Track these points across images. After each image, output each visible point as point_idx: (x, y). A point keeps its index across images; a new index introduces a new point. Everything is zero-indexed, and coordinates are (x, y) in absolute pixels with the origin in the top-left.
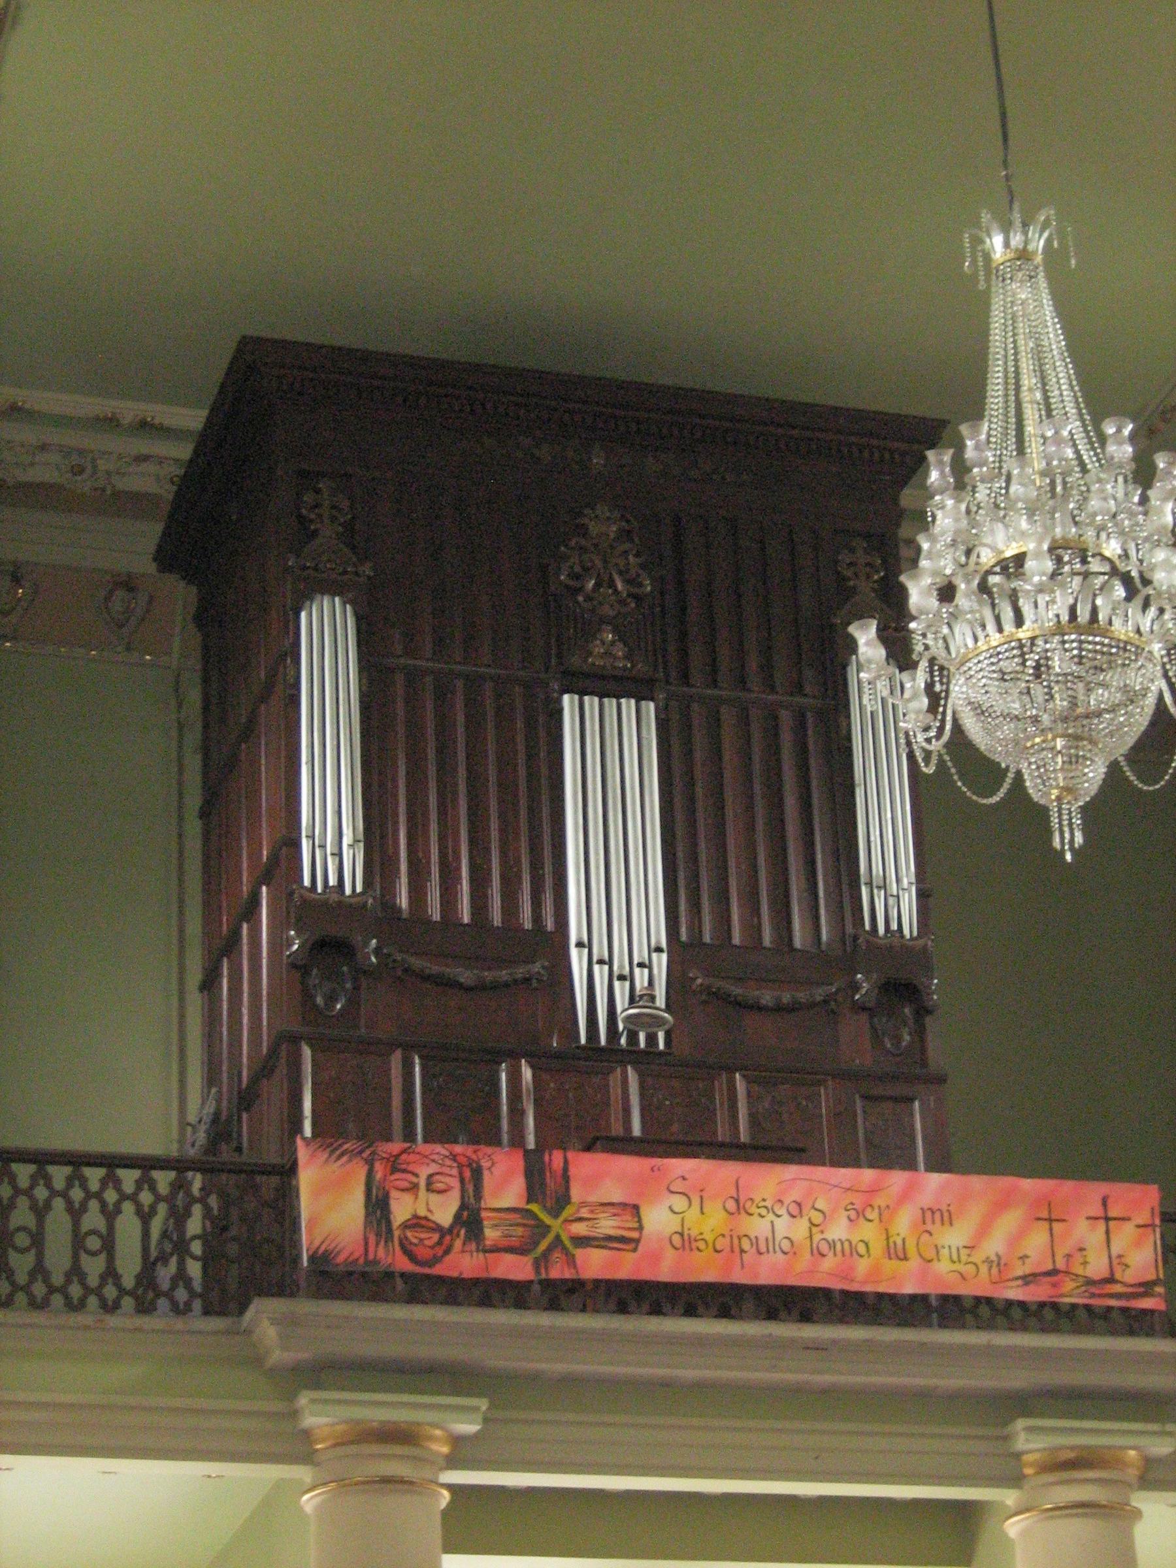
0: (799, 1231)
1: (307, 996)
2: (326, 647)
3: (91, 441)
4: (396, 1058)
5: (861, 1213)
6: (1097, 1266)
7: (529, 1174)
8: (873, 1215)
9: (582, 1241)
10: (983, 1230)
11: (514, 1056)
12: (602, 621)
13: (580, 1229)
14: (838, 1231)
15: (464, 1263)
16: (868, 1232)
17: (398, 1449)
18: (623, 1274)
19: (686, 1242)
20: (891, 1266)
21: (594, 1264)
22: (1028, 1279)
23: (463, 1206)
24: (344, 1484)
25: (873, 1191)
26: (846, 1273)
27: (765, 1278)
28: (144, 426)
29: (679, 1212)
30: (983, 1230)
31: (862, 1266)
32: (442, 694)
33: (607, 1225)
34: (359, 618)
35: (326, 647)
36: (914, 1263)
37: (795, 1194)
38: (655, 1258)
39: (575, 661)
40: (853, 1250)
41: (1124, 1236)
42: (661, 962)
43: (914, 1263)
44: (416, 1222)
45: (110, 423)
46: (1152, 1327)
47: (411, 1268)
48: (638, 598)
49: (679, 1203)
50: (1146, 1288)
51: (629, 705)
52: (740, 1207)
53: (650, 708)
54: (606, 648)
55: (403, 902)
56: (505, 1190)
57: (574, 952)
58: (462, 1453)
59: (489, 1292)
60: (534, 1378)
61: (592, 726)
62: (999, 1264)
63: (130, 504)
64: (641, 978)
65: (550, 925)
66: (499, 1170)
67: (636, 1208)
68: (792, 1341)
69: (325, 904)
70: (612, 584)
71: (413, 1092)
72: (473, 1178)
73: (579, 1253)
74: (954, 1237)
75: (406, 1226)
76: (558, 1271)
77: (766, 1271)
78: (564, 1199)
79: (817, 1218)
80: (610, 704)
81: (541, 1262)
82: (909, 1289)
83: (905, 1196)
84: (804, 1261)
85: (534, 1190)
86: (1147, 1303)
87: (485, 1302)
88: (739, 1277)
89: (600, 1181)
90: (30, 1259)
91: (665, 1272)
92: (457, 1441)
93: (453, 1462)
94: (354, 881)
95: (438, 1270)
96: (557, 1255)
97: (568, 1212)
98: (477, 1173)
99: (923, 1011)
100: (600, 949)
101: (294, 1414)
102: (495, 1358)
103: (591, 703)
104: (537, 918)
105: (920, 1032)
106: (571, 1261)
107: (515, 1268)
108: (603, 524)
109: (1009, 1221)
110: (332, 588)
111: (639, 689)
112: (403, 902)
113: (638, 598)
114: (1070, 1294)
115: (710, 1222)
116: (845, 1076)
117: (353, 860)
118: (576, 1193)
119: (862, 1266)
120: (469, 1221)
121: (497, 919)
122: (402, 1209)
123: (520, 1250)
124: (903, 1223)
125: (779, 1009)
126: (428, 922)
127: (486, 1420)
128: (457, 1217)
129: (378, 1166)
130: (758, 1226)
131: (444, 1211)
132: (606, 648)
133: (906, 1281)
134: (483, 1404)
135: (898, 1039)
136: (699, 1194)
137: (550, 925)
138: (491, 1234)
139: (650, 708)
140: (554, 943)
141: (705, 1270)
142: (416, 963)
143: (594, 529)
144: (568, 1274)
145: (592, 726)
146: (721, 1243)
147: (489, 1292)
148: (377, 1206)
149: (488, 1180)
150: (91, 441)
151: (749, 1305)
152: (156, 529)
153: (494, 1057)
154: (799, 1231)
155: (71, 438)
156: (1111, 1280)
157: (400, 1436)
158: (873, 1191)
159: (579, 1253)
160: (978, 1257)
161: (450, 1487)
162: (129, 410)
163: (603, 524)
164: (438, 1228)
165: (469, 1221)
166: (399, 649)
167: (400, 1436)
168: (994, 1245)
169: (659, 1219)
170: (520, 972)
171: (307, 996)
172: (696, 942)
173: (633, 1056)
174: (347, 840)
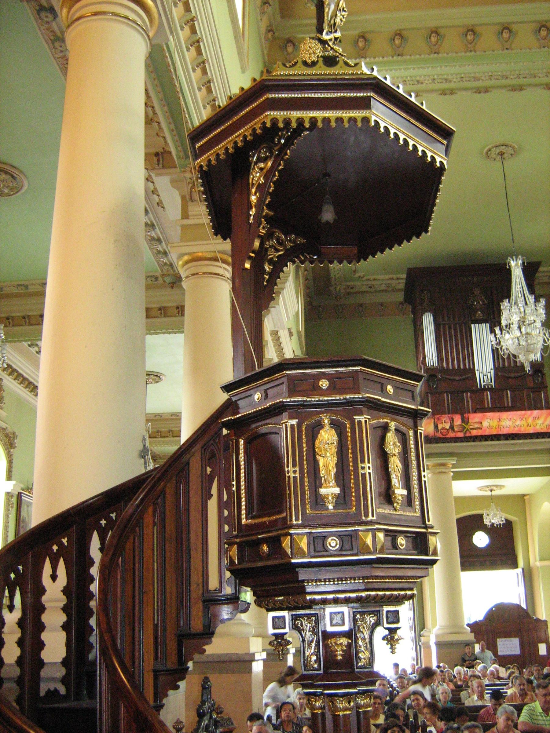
0: (511, 423)
1: (429, 385)
2: (428, 321)
3: (390, 282)
4: (445, 395)
5: (522, 419)
7: (462, 418)
8: (524, 419)
10: (545, 420)
11: (467, 391)
12: (478, 310)
13: (471, 427)
14: (518, 423)
15: (452, 435)
16: (524, 422)
17: (442, 467)
18: (479, 434)
21: (474, 433)
23: (451, 425)
24: (434, 473)
25: (524, 415)
26: (520, 431)
27: (504, 433)
28: (398, 279)
29: (490, 422)
30: (545, 420)
31: (523, 429)
32: (450, 328)
33: (476, 426)
34: (433, 316)
35: (428, 321)
36: (532, 427)
37: (510, 417)
38: (485, 431)
39: (473, 318)
40: (521, 426)
42: (492, 372)
43: (532, 427)
44: (443, 429)
45: (392, 279)
47: (442, 436)
48: (484, 304)
49: (489, 421)
51: (484, 325)
52: (500, 420)
53: (488, 325)
55: (445, 366)
56: (458, 421)
57: (476, 372)
58: (454, 466)
59: (456, 440)
61: (477, 329)
63: (399, 290)
64: (489, 375)
65: (472, 367)
66: (456, 418)
67: (481, 423)
69: (431, 368)
70: (479, 302)
73: (471, 431)
74: (540, 422)
75: (441, 429)
76: (468, 435)
77: (505, 431)
78: (468, 422)
79: (514, 421)
80: (480, 325)
82: (531, 432)
83: (530, 416)
84: (512, 428)
85: (463, 421)
87: (456, 442)
88: (501, 433)
89: (475, 418)
91: (487, 433)
92: (453, 464)
93: (453, 468)
94: (436, 364)
95: (447, 436)
96: (468, 432)
97: (469, 424)
98: (453, 419)
99: (543, 375)
100: (481, 370)
103: (477, 325)
105: (542, 379)
106: (470, 433)
107: (461, 435)
108: (477, 291)
110: (428, 311)
111: (485, 321)
112: (445, 366)
113: (484, 304)
115: (494, 423)
116: (529, 388)
117: (435, 360)
118: (470, 421)
119: (523, 429)
120: (452, 427)
121: (462, 367)
122: (440, 426)
124: (530, 420)
125: (515, 377)
126: (450, 370)
127: (457, 461)
128: (450, 427)
129: (436, 420)
130: (503, 423)
131: (447, 426)
134: (456, 458)
135: (538, 380)
136: (492, 419)
137: (472, 367)
138: (456, 429)
139: (488, 325)
140: (472, 371)
142: (448, 377)
143: (475, 293)
144: (470, 435)
145: (477, 329)
146: (497, 427)
148: (436, 426)
149: (454, 420)
150: (390, 282)
151: (502, 437)
152: (403, 293)
153: (463, 392)
154: (511, 423)
155: (385, 282)
157: (443, 465)
158: (524, 415)
159: (471, 431)
160: (544, 425)
161: (452, 472)
162: (395, 276)
163: (477, 291)
164: (447, 429)
165: (452, 427)
166: (441, 320)
167: (443, 465)
169: (485, 424)
170: (467, 376)
171: (429, 385)
172: (499, 366)
173: (489, 389)
174: (434, 357)
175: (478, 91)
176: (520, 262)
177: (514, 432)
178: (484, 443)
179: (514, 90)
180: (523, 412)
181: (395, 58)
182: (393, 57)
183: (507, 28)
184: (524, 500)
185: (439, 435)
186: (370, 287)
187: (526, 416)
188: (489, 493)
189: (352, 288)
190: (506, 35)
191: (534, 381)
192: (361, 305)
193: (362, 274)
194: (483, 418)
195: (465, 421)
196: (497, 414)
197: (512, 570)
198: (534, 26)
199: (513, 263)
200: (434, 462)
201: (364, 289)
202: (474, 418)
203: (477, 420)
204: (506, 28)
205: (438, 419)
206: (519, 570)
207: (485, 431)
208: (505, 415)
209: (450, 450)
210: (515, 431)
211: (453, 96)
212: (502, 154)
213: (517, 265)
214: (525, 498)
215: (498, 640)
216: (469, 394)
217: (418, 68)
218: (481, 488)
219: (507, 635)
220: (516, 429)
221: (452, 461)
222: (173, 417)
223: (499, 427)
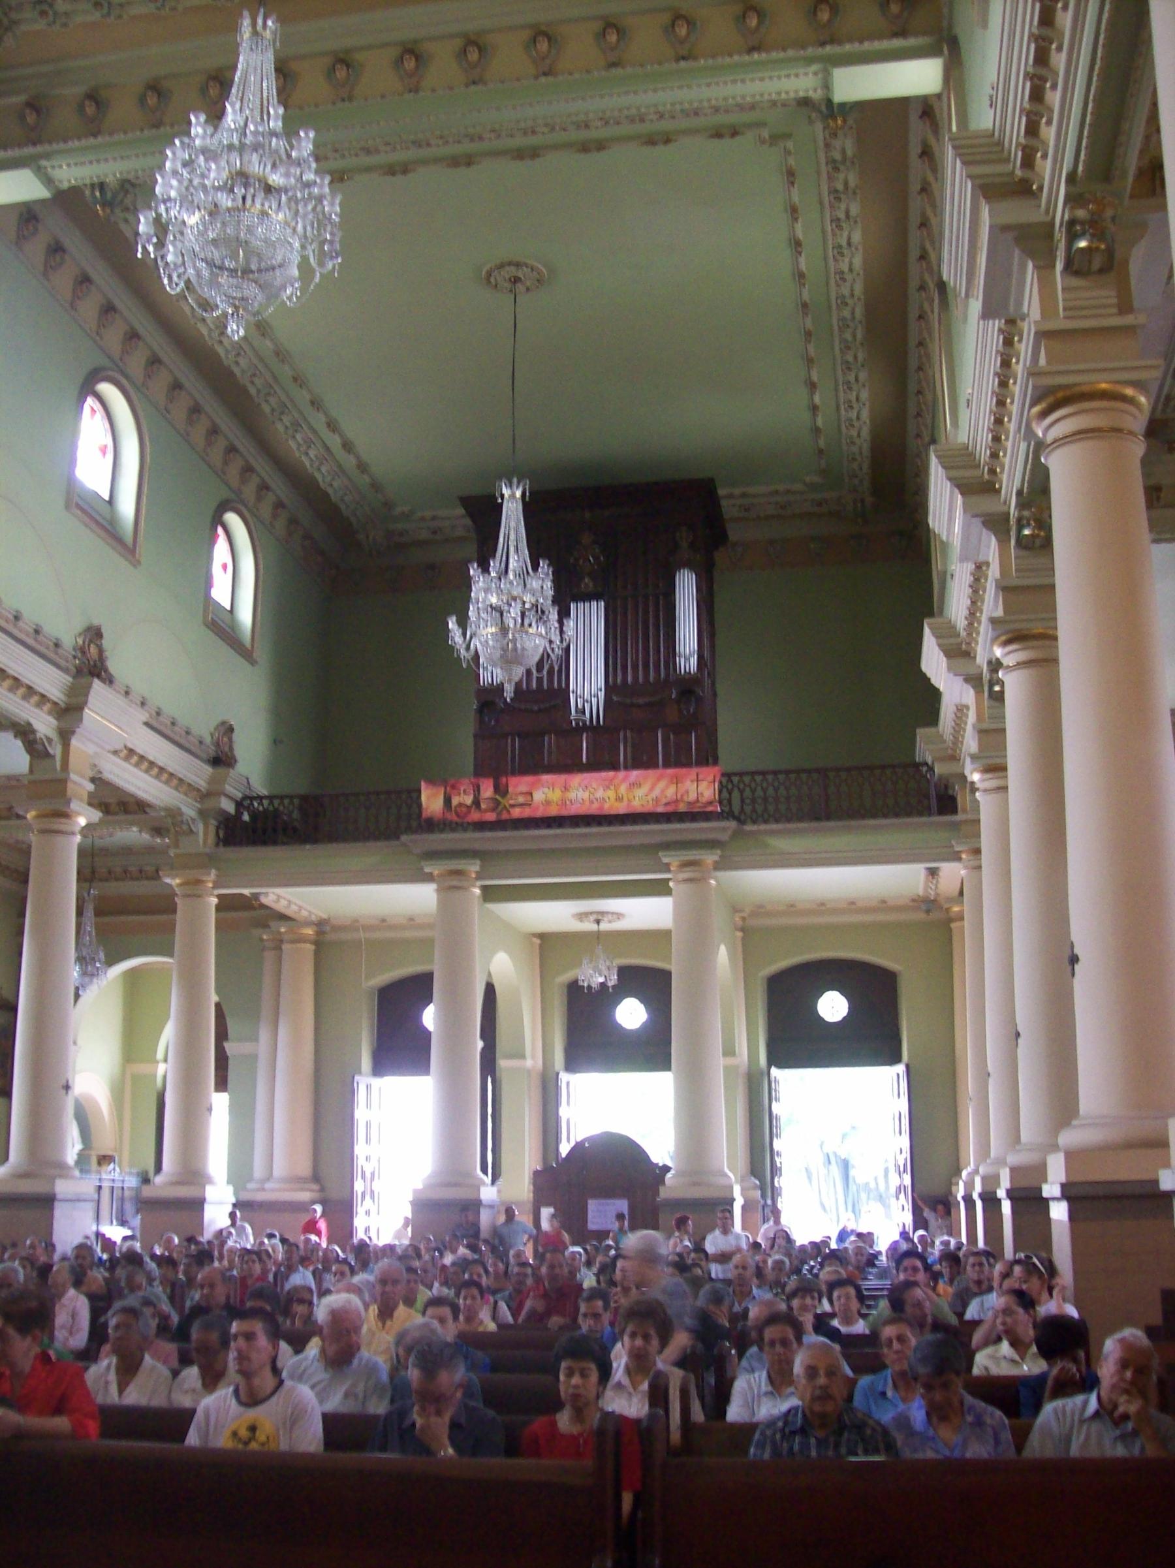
5: (608, 787)
6: (692, 796)
9: (513, 806)
10: (652, 789)
13: (512, 802)
14: (600, 794)
15: (475, 816)
16: (611, 793)
19: (548, 803)
20: (618, 804)
21: (516, 813)
22: (667, 804)
26: (601, 808)
30: (652, 789)
31: (606, 806)
33: (521, 799)
38: (537, 808)
41: (703, 785)
42: (602, 695)
44: (460, 805)
46: (929, 809)
49: (546, 790)
50: (710, 803)
52: (566, 788)
54: (587, 583)
56: (487, 791)
59: (481, 826)
60: (498, 852)
62: (657, 800)
64: (594, 701)
67: (531, 794)
68: (572, 835)
71: (663, 741)
72: (477, 789)
74: (640, 792)
76: (505, 816)
77: (574, 810)
80: (580, 605)
81: (499, 814)
82: (622, 812)
85: (497, 789)
86: (710, 809)
88: (565, 813)
89: (518, 785)
90: (756, 794)
91: (539, 814)
98: (478, 787)
101: (422, 869)
102: (477, 846)
104: (635, 678)
107: (491, 817)
108: (586, 539)
109: (662, 784)
111: (596, 597)
114: (682, 808)
115: (555, 795)
118: (510, 790)
119: (606, 806)
120: (477, 803)
122: (455, 801)
123: (493, 810)
124: (623, 789)
128: (473, 802)
130: (572, 795)
131: (469, 800)
132: (587, 583)
133: (621, 808)
134: (719, 852)
136: (553, 786)
138: (483, 806)
141: (553, 811)
145: (581, 611)
147: (481, 826)
148: (448, 801)
154: (586, 795)
156: (698, 801)
157: (458, 873)
160: (649, 798)
163: (586, 539)
168: (657, 792)
169: (538, 796)
173: (585, 728)
175: (651, 141)
176: (518, 494)
177: (589, 812)
178: (629, 828)
179: (718, 135)
180: (611, 774)
181: (146, 132)
182: (142, 130)
183: (614, 26)
184: (951, 930)
185: (452, 817)
186: (435, 532)
187: (616, 782)
188: (594, 927)
189: (435, 532)
190: (410, 64)
191: (680, 711)
192: (432, 567)
193: (406, 509)
194: (533, 785)
195: (501, 790)
196: (561, 778)
197: (888, 1068)
198: (526, 34)
199: (506, 492)
200: (682, 858)
201: (424, 535)
202: (516, 786)
203: (523, 788)
204: (343, 60)
205: (453, 787)
206: (900, 1068)
207: (537, 808)
208: (577, 779)
209: (466, 846)
210: (593, 809)
211: (738, 138)
212: (516, 280)
213: (513, 496)
214: (953, 925)
215: (590, 1202)
216: (629, 734)
217: (145, 155)
218: (582, 916)
219: (608, 1193)
220: (596, 805)
221: (474, 867)
222: (14, 783)
223: (563, 803)
